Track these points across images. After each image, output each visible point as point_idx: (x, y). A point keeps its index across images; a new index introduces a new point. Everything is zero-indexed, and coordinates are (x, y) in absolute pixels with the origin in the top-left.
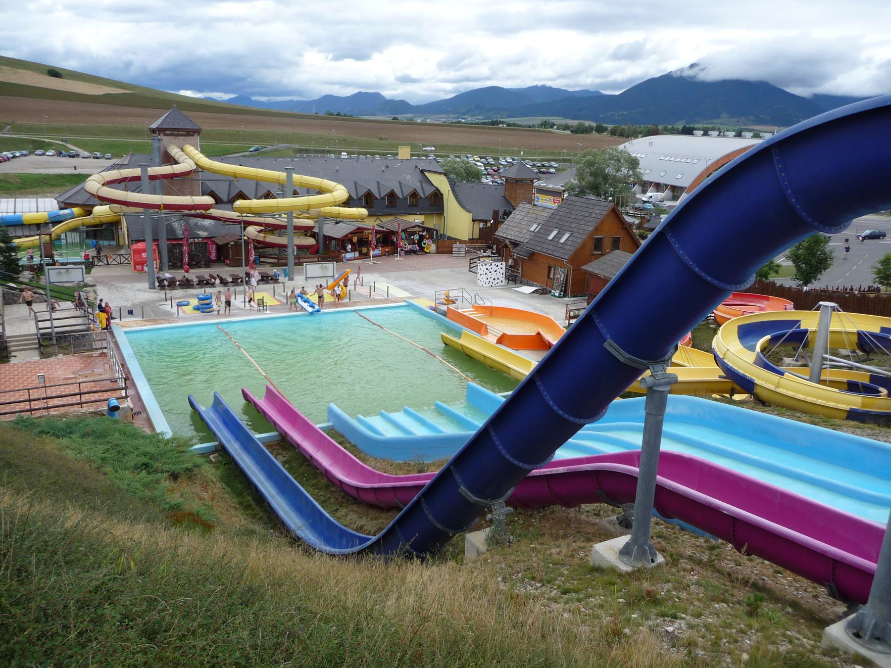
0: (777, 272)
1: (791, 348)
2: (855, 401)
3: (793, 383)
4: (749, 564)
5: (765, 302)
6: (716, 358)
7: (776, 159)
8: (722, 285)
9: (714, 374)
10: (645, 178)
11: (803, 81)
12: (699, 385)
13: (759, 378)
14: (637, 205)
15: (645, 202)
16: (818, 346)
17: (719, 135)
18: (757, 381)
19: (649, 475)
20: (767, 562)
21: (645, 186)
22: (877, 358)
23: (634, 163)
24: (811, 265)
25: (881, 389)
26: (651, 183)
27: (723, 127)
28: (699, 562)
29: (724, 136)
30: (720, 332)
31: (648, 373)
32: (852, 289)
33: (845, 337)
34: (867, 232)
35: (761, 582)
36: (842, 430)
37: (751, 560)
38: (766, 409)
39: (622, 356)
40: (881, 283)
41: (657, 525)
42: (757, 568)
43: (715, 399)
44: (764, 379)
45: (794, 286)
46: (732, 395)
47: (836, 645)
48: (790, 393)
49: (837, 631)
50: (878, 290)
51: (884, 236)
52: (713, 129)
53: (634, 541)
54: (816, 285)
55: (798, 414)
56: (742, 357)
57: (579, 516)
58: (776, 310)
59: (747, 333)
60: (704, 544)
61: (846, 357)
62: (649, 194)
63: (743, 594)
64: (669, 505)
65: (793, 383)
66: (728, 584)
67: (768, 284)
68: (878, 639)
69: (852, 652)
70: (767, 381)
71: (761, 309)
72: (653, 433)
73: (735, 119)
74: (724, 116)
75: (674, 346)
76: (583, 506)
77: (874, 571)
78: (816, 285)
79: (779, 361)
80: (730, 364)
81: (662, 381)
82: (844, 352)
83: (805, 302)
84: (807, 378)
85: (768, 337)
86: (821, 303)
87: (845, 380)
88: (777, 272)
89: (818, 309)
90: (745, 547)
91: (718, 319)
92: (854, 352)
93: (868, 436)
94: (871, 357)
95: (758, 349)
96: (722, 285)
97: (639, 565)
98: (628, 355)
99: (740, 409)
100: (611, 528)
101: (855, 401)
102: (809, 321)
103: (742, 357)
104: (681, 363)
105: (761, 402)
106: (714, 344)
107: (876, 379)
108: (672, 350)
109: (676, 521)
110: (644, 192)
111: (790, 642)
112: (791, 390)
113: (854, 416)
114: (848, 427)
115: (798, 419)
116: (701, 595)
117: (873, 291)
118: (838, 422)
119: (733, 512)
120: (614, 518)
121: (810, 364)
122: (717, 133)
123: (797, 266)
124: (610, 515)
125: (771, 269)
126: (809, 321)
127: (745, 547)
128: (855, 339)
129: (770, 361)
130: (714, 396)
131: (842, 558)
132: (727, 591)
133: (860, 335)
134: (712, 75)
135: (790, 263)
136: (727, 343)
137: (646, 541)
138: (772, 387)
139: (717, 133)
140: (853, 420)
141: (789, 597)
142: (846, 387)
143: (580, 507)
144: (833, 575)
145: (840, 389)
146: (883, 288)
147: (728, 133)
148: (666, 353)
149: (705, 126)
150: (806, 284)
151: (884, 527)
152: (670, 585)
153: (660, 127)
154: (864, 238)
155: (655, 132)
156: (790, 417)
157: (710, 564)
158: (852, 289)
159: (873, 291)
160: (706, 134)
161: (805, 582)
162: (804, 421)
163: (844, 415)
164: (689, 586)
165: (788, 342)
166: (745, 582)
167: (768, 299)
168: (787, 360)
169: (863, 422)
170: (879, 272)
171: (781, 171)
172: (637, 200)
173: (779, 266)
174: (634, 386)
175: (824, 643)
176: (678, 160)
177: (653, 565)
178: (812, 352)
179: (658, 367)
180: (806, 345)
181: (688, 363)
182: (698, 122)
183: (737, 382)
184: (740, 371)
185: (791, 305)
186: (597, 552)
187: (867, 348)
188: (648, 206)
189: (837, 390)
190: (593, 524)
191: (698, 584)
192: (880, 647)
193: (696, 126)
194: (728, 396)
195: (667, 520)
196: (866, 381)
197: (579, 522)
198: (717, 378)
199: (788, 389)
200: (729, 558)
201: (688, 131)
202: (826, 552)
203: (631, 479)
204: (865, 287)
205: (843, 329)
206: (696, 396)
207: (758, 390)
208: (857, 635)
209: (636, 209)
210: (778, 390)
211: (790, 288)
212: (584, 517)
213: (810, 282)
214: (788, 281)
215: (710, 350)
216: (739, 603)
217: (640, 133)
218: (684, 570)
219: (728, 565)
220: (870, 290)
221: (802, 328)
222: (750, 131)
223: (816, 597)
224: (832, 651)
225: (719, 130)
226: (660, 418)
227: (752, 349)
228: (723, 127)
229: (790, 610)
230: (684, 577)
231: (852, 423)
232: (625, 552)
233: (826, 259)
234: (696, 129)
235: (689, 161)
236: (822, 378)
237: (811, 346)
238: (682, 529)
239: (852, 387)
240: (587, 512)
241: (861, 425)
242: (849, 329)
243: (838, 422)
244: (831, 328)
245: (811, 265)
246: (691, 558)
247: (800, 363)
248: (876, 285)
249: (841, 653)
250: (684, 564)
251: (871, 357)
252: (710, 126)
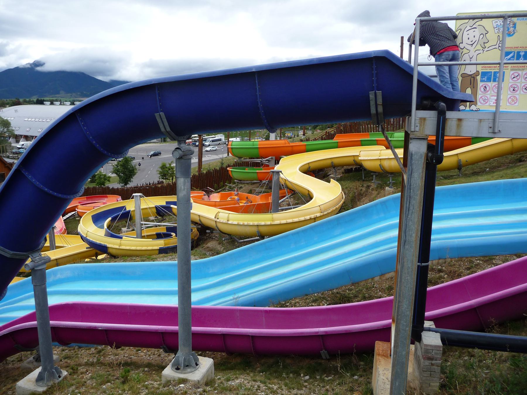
0: (109, 181)
1: (124, 222)
2: (161, 243)
3: (129, 242)
4: (122, 352)
5: (106, 199)
6: (82, 237)
7: (79, 119)
8: (65, 196)
9: (83, 247)
10: (16, 133)
11: (101, 73)
12: (76, 256)
13: (109, 244)
14: (14, 151)
15: (19, 148)
16: (137, 218)
17: (61, 104)
18: (108, 245)
19: (44, 323)
20: (132, 348)
21: (17, 138)
22: (167, 218)
23: (6, 124)
24: (126, 175)
25: (172, 234)
26: (21, 136)
27: (62, 99)
28: (92, 364)
29: (64, 104)
30: (81, 222)
31: (30, 260)
32: (150, 184)
33: (149, 210)
34: (152, 153)
35: (129, 360)
36: (157, 261)
37: (123, 350)
38: (116, 260)
39: (8, 253)
40: (163, 179)
41: (57, 353)
42: (127, 353)
43: (87, 262)
44: (112, 243)
45: (120, 187)
46: (96, 257)
47: (169, 379)
48: (128, 248)
49: (168, 372)
50: (162, 182)
51: (160, 154)
52: (57, 101)
53: (44, 370)
54: (131, 185)
55: (134, 258)
56: (97, 233)
57: (7, 367)
58: (112, 203)
59: (97, 219)
60: (94, 352)
61: (153, 221)
62: (21, 143)
63: (119, 372)
64: (63, 337)
65: (129, 242)
66: (110, 370)
67: (105, 189)
68: (187, 366)
69: (177, 379)
70: (114, 244)
71: (104, 203)
72: (41, 296)
73: (69, 94)
74: (62, 93)
75: (44, 238)
76: (8, 358)
77: (178, 331)
78: (131, 185)
79: (119, 231)
80: (91, 239)
81: (40, 262)
82: (152, 218)
83: (126, 195)
84: (135, 237)
85: (110, 219)
86: (134, 194)
87: (155, 233)
88: (109, 181)
89: (133, 198)
90: (114, 345)
91: (80, 214)
92: (156, 217)
93: (170, 260)
94: (164, 218)
95: (105, 227)
96: (65, 196)
97: (51, 383)
98: (12, 252)
99: (104, 265)
100: (31, 366)
101: (161, 243)
102: (130, 205)
103: (97, 233)
104: (62, 245)
105: (113, 257)
106: (79, 230)
107: (169, 229)
108: (43, 242)
109: (73, 344)
110: (18, 142)
111: (147, 388)
112: (128, 246)
113: (163, 251)
114: (159, 258)
115: (135, 261)
116: (94, 384)
117: (160, 183)
118: (154, 256)
119: (104, 327)
120: (31, 358)
121: (135, 229)
122: (59, 103)
123: (119, 175)
124: (29, 357)
125: (105, 179)
126: (130, 205)
127: (114, 345)
128: (155, 210)
129: (114, 232)
130: (86, 260)
131: (166, 330)
132: (110, 375)
133: (156, 207)
134: (50, 67)
135: (114, 175)
136: (88, 228)
137: (52, 367)
138: (117, 247)
139: (59, 103)
140: (162, 253)
141: (146, 362)
142: (156, 237)
143: (6, 360)
144: (164, 341)
145: (153, 239)
146: (164, 181)
147: (66, 103)
148: (39, 245)
149: (51, 99)
150: (126, 184)
151: (177, 306)
152: (74, 387)
153: (21, 100)
154: (151, 156)
155: (18, 104)
156: (130, 261)
157: (100, 363)
158: (150, 184)
159: (160, 183)
160: (52, 104)
161: (153, 350)
162: (138, 261)
163: (157, 252)
164: (86, 382)
165: (120, 220)
166: (119, 365)
167: (107, 197)
168: (124, 229)
169: (167, 253)
170: (161, 173)
171: (84, 126)
172: (13, 148)
173: (110, 177)
174: (23, 269)
175: (163, 381)
176: (37, 120)
177: (60, 379)
178: (135, 222)
179: (36, 255)
180: (131, 219)
181: (62, 244)
182: (46, 96)
183: (97, 249)
184: (98, 242)
185: (120, 198)
186: (20, 387)
187: (161, 214)
188: (21, 150)
189: (151, 240)
190: (18, 368)
191: (92, 378)
192: (189, 370)
193: (45, 99)
194: (94, 258)
195: (69, 345)
196: (165, 231)
197: (7, 371)
198: (85, 250)
199: (126, 246)
200: (110, 353)
201: (40, 102)
202: (157, 330)
203: (34, 330)
204: (156, 181)
205: (148, 207)
206: (74, 263)
207: (110, 251)
208: (178, 369)
209: (14, 153)
210: (121, 248)
211: (118, 189)
212: (10, 366)
213: (128, 184)
214: (116, 185)
215: (78, 234)
216: (117, 378)
217: (8, 104)
218: (82, 373)
219: (111, 358)
220: (159, 183)
221: (127, 210)
222: (47, 101)
223: (159, 355)
224: (168, 383)
225: (60, 101)
226: (43, 286)
227: (102, 227)
228: (62, 99)
229: (146, 369)
230: (83, 377)
231: (162, 255)
232: (40, 379)
233: (133, 170)
234: (45, 101)
235: (44, 120)
236: (143, 235)
237: (133, 218)
238: (80, 347)
239: (159, 236)
240: (13, 361)
241: (166, 255)
242: (151, 206)
243: (154, 256)
244: (142, 207)
245: (126, 175)
246: (87, 364)
247: (131, 229)
248: (161, 180)
249: (172, 382)
250: (82, 369)
251: (164, 218)
252: (54, 99)
